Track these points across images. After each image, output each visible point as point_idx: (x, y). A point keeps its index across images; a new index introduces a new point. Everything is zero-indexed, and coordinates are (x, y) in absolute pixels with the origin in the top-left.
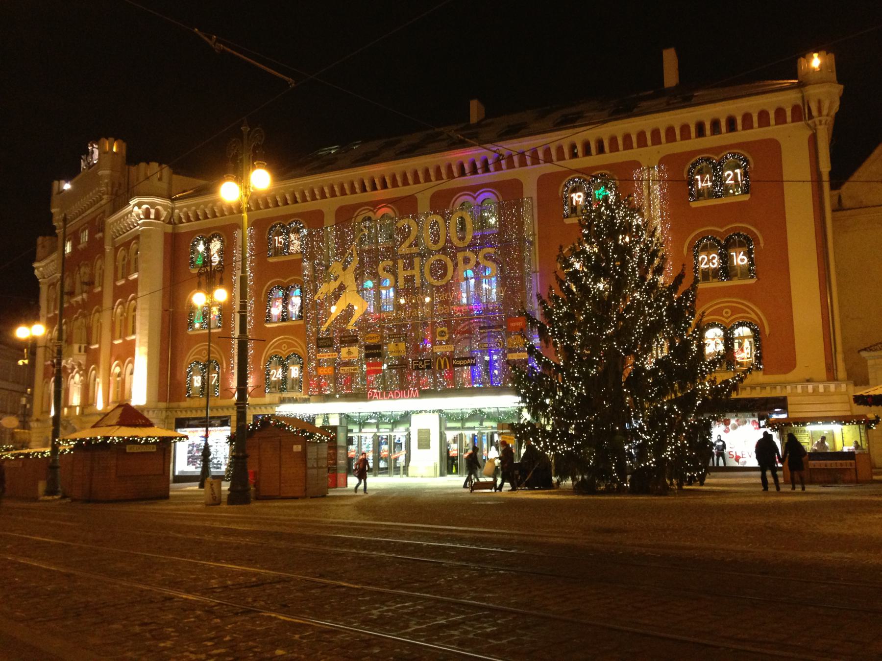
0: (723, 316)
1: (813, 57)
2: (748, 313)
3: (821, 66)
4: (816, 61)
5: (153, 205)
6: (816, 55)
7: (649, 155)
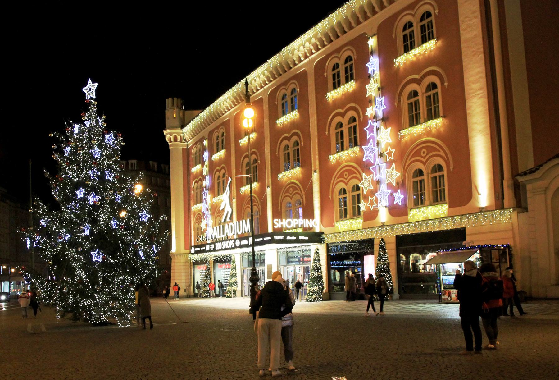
0: (344, 178)
2: (439, 151)
5: (178, 133)
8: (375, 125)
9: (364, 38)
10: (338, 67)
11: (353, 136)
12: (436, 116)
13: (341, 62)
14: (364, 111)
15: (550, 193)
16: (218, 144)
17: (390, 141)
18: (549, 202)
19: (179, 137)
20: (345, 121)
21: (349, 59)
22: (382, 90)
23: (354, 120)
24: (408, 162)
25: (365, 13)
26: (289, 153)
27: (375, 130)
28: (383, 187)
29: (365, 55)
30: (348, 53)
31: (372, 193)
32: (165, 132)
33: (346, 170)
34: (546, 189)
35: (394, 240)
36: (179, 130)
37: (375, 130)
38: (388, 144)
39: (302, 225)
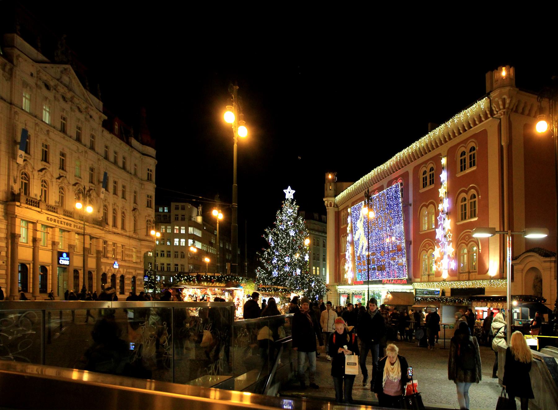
1: (502, 70)
3: (506, 77)
4: (504, 73)
6: (504, 68)
7: (444, 149)
8: (443, 216)
9: (437, 159)
10: (464, 155)
11: (464, 212)
12: (475, 216)
13: (467, 150)
14: (438, 207)
15: (524, 272)
16: (425, 179)
17: (450, 228)
18: (524, 276)
19: (333, 204)
20: (468, 197)
21: (473, 149)
22: (448, 194)
23: (475, 197)
24: (459, 243)
25: (459, 130)
26: (465, 205)
27: (442, 219)
28: (446, 257)
29: (440, 169)
30: (473, 144)
31: (442, 258)
32: (324, 200)
33: (427, 243)
34: (522, 270)
35: (449, 291)
36: (332, 199)
37: (442, 219)
38: (449, 230)
39: (209, 298)
